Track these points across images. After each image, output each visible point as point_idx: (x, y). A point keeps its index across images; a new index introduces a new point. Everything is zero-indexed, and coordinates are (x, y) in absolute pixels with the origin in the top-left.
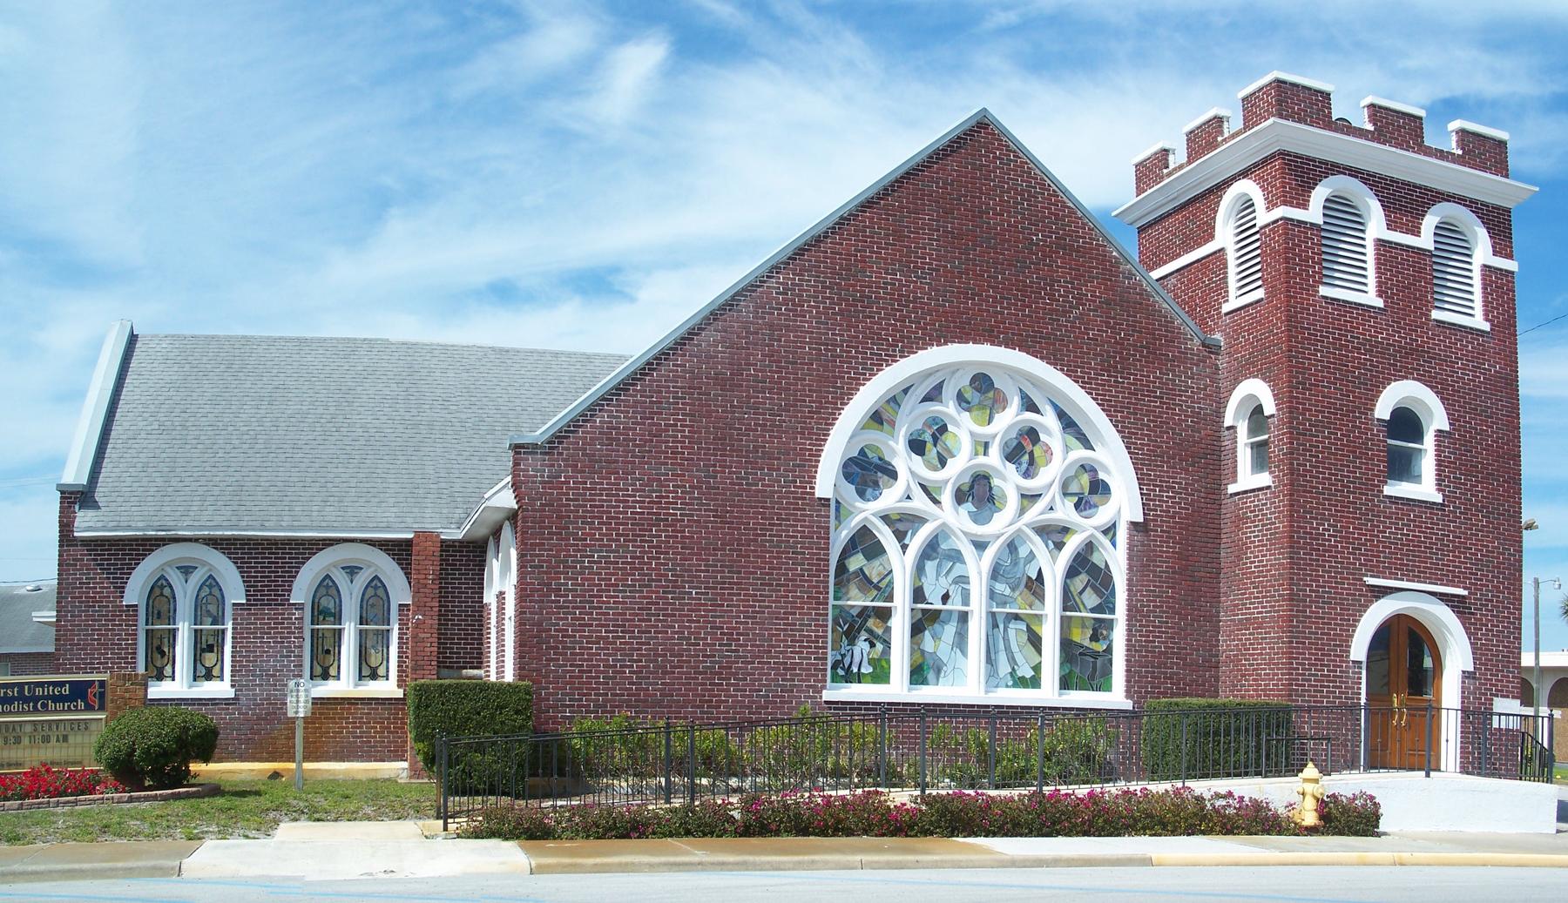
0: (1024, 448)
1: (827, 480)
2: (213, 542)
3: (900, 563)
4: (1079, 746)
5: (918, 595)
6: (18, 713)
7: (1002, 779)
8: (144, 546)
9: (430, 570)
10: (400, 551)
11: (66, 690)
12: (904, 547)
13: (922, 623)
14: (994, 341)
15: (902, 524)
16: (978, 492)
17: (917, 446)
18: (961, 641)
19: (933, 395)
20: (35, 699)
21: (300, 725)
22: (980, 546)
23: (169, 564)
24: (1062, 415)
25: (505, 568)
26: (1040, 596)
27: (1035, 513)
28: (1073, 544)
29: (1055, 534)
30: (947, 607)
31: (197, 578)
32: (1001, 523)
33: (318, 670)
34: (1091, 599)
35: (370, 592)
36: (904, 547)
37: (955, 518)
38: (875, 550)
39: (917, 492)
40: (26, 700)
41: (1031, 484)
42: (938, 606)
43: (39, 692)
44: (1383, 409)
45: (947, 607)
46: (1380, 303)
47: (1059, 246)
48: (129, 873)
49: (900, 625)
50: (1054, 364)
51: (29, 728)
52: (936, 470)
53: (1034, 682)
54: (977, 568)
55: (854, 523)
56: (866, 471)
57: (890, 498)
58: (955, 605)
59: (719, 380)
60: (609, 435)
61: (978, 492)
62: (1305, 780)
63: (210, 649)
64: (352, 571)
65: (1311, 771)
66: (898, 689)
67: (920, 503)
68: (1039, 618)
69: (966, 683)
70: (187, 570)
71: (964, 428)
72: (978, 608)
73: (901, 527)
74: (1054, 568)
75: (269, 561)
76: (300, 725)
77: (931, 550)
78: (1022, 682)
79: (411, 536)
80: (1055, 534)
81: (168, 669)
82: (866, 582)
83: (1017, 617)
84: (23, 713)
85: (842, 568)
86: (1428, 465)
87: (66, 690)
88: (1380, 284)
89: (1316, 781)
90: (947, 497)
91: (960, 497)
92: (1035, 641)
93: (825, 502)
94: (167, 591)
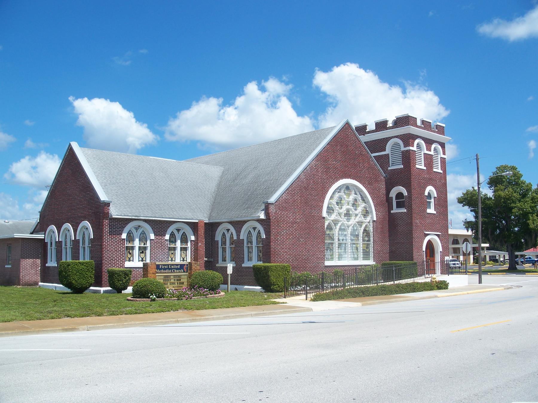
0: (355, 204)
1: (324, 214)
2: (145, 221)
5: (339, 240)
6: (168, 273)
8: (127, 221)
9: (202, 231)
10: (194, 226)
11: (179, 267)
20: (172, 269)
21: (229, 276)
24: (362, 198)
25: (530, 267)
26: (358, 239)
31: (140, 231)
34: (366, 239)
35: (183, 236)
40: (169, 269)
43: (172, 267)
44: (426, 194)
46: (425, 168)
48: (242, 316)
49: (336, 245)
51: (172, 277)
56: (330, 210)
58: (344, 242)
63: (142, 252)
64: (178, 230)
67: (338, 218)
68: (358, 244)
75: (160, 227)
76: (229, 276)
79: (197, 221)
81: (132, 258)
84: (170, 273)
86: (432, 205)
87: (179, 267)
88: (425, 164)
94: (131, 235)
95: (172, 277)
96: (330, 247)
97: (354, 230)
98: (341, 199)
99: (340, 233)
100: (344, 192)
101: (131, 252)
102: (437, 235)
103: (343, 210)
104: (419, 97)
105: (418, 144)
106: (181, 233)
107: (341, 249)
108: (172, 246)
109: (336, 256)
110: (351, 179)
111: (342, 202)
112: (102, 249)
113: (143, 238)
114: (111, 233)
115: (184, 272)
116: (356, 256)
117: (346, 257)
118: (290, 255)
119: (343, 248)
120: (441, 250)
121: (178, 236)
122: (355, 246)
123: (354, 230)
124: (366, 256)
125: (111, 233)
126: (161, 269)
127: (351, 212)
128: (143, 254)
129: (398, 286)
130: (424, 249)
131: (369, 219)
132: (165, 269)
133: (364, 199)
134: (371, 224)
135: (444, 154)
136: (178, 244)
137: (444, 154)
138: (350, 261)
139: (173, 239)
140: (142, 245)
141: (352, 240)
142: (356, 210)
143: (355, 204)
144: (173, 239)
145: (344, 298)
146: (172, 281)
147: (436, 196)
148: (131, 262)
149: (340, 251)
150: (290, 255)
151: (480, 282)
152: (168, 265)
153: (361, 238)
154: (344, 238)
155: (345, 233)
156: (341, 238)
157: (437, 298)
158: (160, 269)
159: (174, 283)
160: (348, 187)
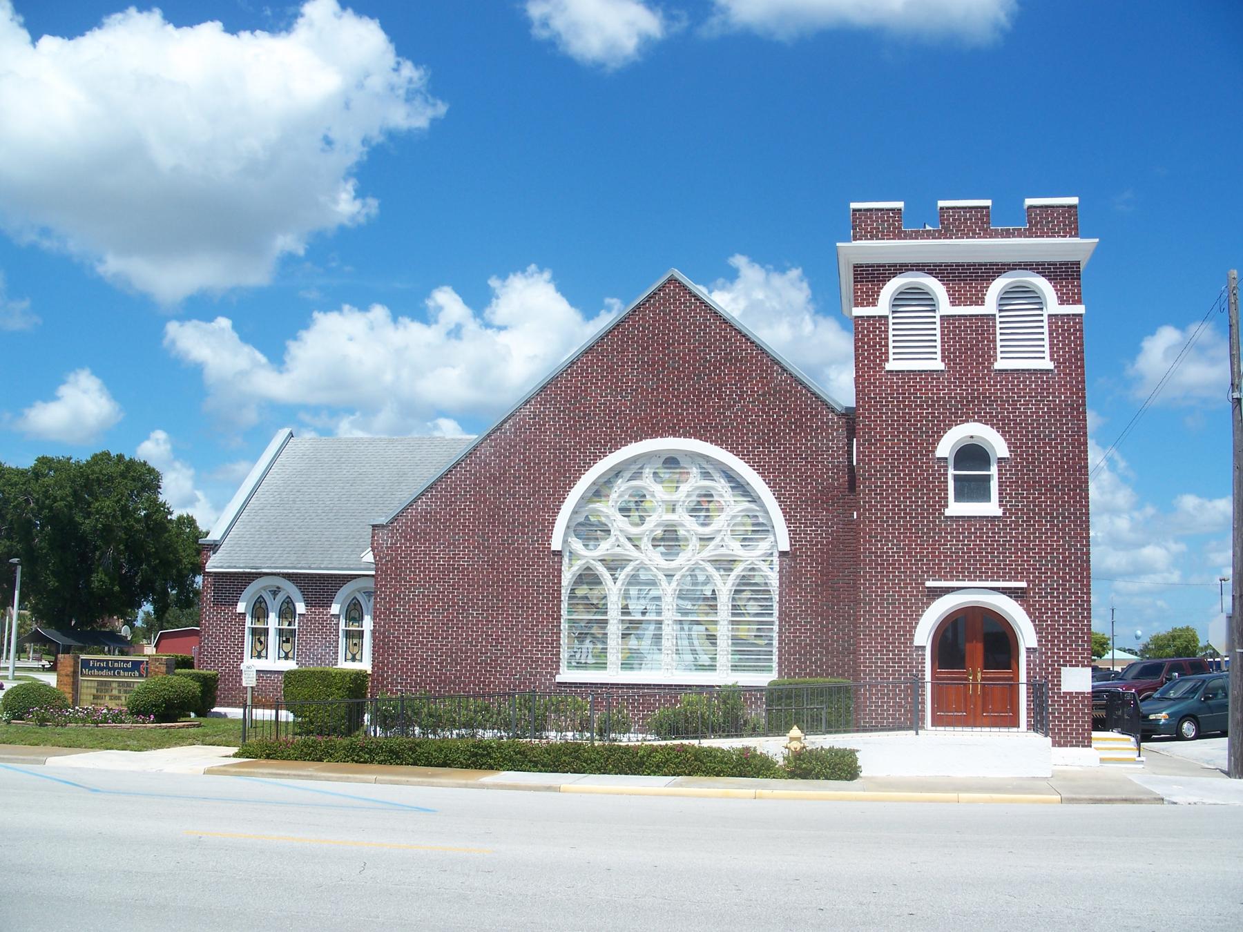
0: (702, 507)
3: (613, 590)
4: (729, 711)
5: (625, 611)
7: (683, 735)
11: (130, 665)
12: (615, 580)
13: (631, 628)
14: (675, 434)
15: (614, 564)
16: (669, 539)
17: (624, 510)
18: (658, 638)
19: (637, 475)
20: (114, 669)
22: (669, 576)
23: (264, 588)
26: (714, 608)
27: (710, 551)
28: (739, 570)
29: (724, 565)
30: (646, 618)
31: (281, 597)
32: (683, 560)
33: (349, 656)
34: (753, 607)
36: (615, 580)
37: (654, 558)
38: (595, 581)
39: (623, 540)
40: (110, 669)
41: (646, 544)
42: (639, 617)
45: (646, 618)
47: (726, 359)
49: (614, 629)
50: (721, 445)
51: (114, 685)
52: (637, 525)
53: (712, 668)
54: (668, 590)
55: (578, 565)
57: (605, 547)
58: (651, 617)
59: (493, 479)
60: (426, 517)
61: (669, 539)
62: (792, 739)
63: (287, 641)
65: (795, 732)
66: (613, 674)
68: (715, 623)
69: (664, 669)
70: (275, 593)
71: (658, 492)
72: (669, 615)
73: (612, 565)
74: (724, 587)
76: (249, 690)
77: (633, 580)
78: (702, 668)
80: (724, 565)
82: (590, 606)
83: (698, 623)
85: (572, 596)
89: (798, 739)
90: (646, 544)
91: (656, 542)
92: (712, 638)
93: (559, 554)
95: (114, 685)
96: (592, 632)
101: (262, 639)
106: (281, 597)
107: (639, 638)
108: (354, 627)
109: (614, 657)
111: (646, 505)
113: (287, 612)
114: (217, 603)
115: (141, 676)
116: (704, 659)
120: (1033, 643)
121: (274, 606)
124: (745, 655)
125: (217, 603)
126: (93, 668)
127: (681, 532)
128: (289, 645)
129: (710, 752)
131: (764, 546)
133: (740, 487)
134: (776, 559)
136: (273, 622)
138: (676, 672)
139: (355, 614)
140: (285, 626)
143: (702, 507)
144: (355, 614)
145: (320, 760)
146: (115, 692)
147: (1006, 454)
148: (263, 660)
152: (107, 661)
155: (654, 593)
157: (553, 794)
158: (91, 669)
159: (119, 698)
160: (671, 461)
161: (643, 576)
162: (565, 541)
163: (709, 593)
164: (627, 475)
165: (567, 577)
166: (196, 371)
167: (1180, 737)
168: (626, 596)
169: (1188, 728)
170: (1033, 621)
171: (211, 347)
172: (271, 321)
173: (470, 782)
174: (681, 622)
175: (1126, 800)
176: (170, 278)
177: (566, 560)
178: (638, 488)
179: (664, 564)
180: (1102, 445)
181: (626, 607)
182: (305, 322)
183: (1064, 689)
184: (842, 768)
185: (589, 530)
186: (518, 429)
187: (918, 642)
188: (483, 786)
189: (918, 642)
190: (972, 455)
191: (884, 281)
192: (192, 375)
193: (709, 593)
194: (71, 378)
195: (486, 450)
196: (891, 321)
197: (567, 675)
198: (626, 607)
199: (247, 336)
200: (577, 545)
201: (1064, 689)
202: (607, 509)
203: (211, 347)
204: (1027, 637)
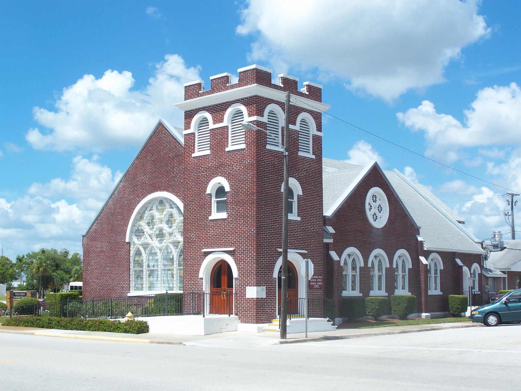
5: (149, 266)
13: (151, 273)
37: (155, 243)
40: (20, 296)
49: (145, 273)
58: (155, 268)
60: (96, 231)
61: (161, 235)
72: (160, 267)
93: (129, 243)
96: (139, 276)
97: (168, 253)
98: (152, 218)
99: (151, 258)
100: (157, 209)
102: (299, 253)
103: (155, 231)
104: (169, 65)
105: (303, 121)
107: (153, 277)
109: (146, 285)
110: (161, 191)
111: (154, 221)
112: (257, 260)
116: (171, 285)
117: (157, 287)
118: (98, 284)
119: (156, 276)
120: (411, 267)
122: (170, 272)
123: (168, 253)
127: (164, 232)
130: (276, 275)
132: (18, 296)
135: (319, 129)
137: (319, 129)
141: (165, 265)
142: (171, 227)
149: (151, 279)
150: (98, 284)
151: (284, 332)
153: (176, 263)
154: (156, 264)
155: (156, 258)
156: (151, 264)
160: (161, 202)
161: (153, 251)
162: (131, 238)
163: (171, 257)
164: (149, 209)
165: (132, 253)
166: (422, 133)
167: (487, 324)
168: (149, 260)
169: (492, 319)
170: (237, 266)
171: (424, 117)
172: (454, 100)
173: (21, 331)
174: (164, 270)
175: (168, 343)
176: (388, 87)
177: (132, 246)
178: (151, 213)
179: (159, 245)
180: (390, 169)
181: (148, 265)
182: (473, 98)
183: (247, 297)
184: (143, 329)
185: (139, 233)
186: (119, 193)
187: (201, 276)
188: (26, 334)
189: (200, 276)
190: (220, 191)
191: (225, 110)
192: (420, 136)
193: (171, 257)
194: (355, 146)
195: (111, 203)
196: (230, 128)
197: (133, 293)
198: (148, 265)
199: (440, 110)
200: (135, 239)
201: (247, 297)
202: (143, 224)
203: (424, 117)
204: (235, 274)
